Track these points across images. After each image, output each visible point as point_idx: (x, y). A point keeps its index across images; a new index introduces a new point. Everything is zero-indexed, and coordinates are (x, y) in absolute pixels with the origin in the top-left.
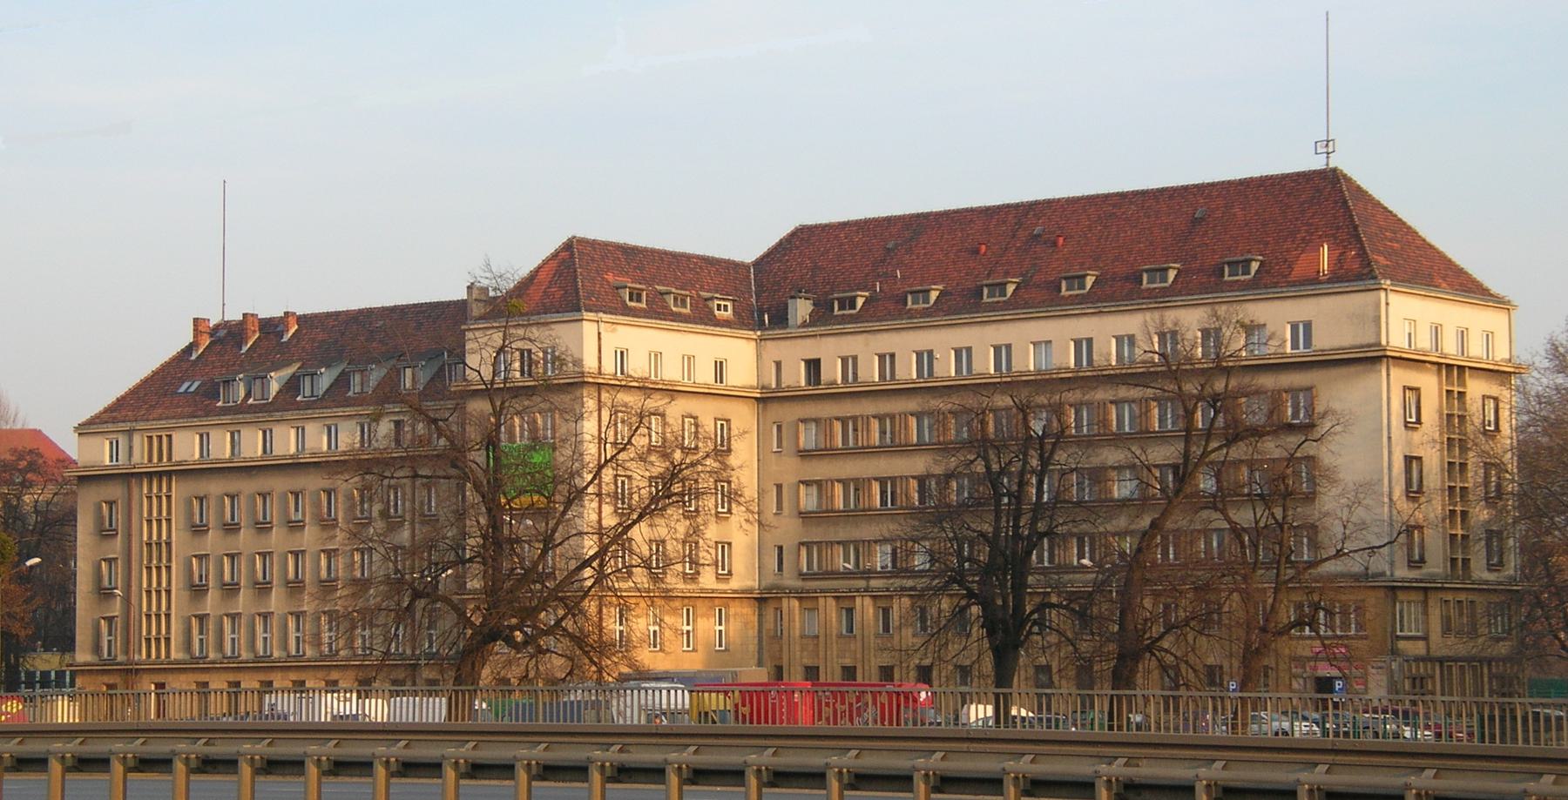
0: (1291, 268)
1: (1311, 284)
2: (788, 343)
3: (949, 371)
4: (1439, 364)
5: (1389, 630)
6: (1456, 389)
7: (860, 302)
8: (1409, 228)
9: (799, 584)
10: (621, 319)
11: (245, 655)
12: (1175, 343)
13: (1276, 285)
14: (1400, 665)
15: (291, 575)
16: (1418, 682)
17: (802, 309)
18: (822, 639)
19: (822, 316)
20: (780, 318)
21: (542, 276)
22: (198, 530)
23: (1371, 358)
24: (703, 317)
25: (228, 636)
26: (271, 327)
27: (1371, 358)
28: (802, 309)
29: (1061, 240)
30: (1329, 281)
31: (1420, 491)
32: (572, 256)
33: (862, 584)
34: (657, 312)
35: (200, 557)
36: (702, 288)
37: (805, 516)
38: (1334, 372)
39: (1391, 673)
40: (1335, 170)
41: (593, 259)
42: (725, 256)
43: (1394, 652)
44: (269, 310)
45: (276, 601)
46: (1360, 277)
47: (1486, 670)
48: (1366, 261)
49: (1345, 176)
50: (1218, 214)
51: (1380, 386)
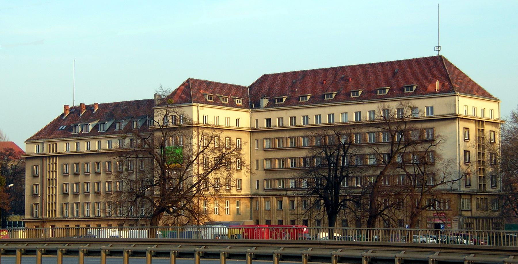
0: (426, 88)
1: (433, 94)
4: (475, 120)
6: (481, 128)
7: (284, 100)
8: (466, 75)
9: (264, 193)
10: (205, 105)
13: (421, 94)
14: (463, 220)
15: (96, 190)
16: (468, 225)
17: (265, 102)
18: (271, 211)
19: (272, 104)
20: (258, 105)
22: (66, 175)
23: (453, 118)
24: (232, 105)
26: (89, 108)
27: (453, 118)
28: (265, 102)
29: (350, 79)
30: (439, 93)
31: (469, 162)
34: (217, 103)
35: (66, 184)
36: (232, 95)
37: (266, 170)
38: (441, 123)
40: (441, 56)
42: (240, 85)
43: (461, 215)
44: (89, 102)
46: (449, 91)
47: (491, 221)
48: (451, 86)
49: (444, 58)
50: (402, 71)
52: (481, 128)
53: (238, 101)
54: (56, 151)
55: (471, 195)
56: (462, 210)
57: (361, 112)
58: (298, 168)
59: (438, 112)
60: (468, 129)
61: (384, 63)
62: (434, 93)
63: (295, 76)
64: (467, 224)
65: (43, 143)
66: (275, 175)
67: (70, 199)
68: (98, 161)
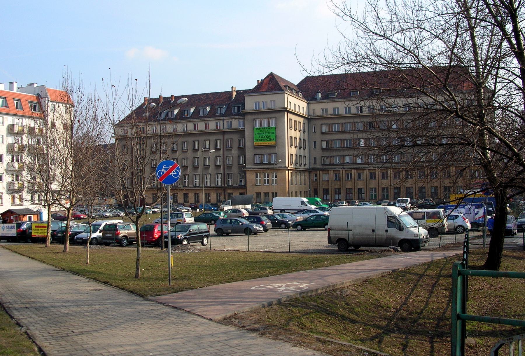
2: (318, 104)
9: (322, 167)
12: (327, 111)
18: (330, 182)
19: (325, 97)
21: (265, 82)
33: (342, 167)
37: (323, 150)
54: (198, 129)
58: (353, 147)
65: (223, 120)
66: (332, 153)
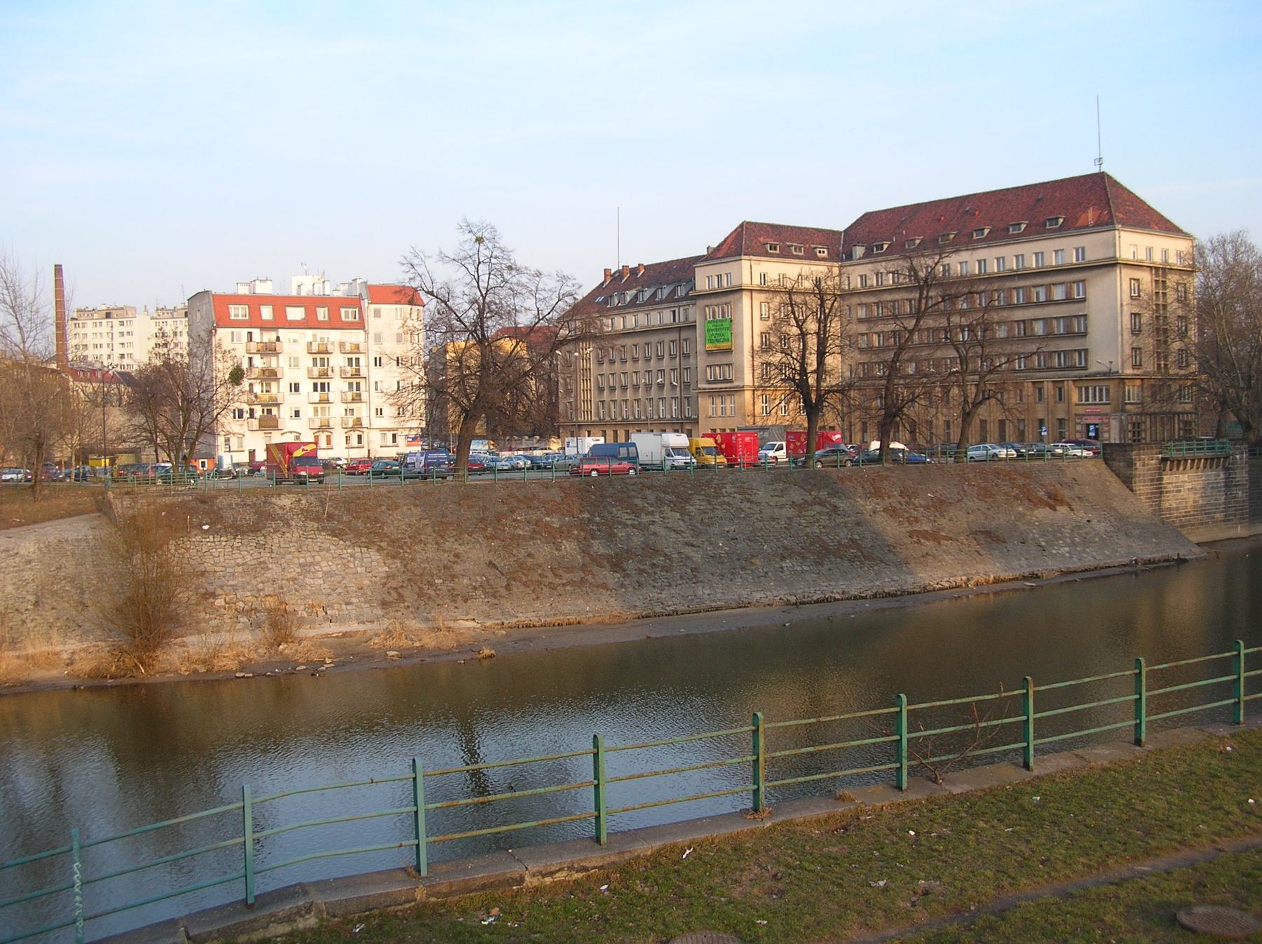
0: (1077, 220)
1: (1084, 229)
3: (1032, 265)
4: (1151, 267)
5: (1121, 399)
6: (1161, 279)
7: (885, 247)
8: (1141, 200)
10: (762, 258)
11: (607, 419)
13: (1069, 229)
14: (1127, 418)
15: (635, 383)
16: (1136, 425)
17: (859, 251)
20: (850, 256)
22: (600, 363)
23: (1111, 264)
24: (811, 256)
25: (613, 410)
26: (634, 271)
27: (1111, 264)
28: (859, 251)
29: (977, 213)
30: (1093, 226)
31: (1140, 330)
32: (742, 230)
34: (786, 254)
35: (601, 375)
36: (813, 243)
38: (1095, 272)
39: (1121, 421)
40: (1103, 172)
41: (753, 231)
42: (829, 228)
43: (1123, 411)
44: (633, 264)
45: (641, 394)
46: (1107, 224)
47: (1176, 418)
48: (1111, 216)
49: (1108, 176)
50: (1049, 196)
51: (1116, 280)
52: (1161, 279)
53: (820, 252)
55: (1142, 379)
56: (1126, 404)
57: (298, 358)
59: (1093, 255)
60: (1137, 280)
61: (1026, 186)
62: (1087, 227)
63: (906, 212)
64: (1134, 424)
67: (606, 395)
68: (647, 342)
